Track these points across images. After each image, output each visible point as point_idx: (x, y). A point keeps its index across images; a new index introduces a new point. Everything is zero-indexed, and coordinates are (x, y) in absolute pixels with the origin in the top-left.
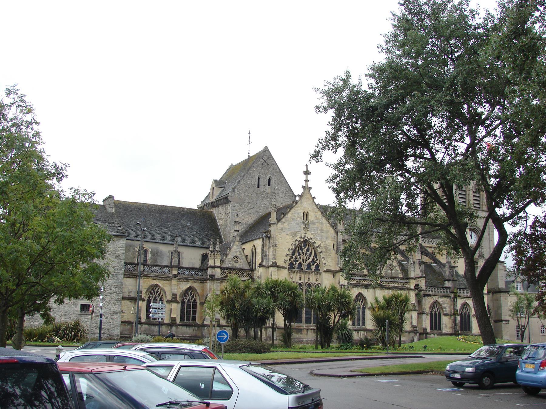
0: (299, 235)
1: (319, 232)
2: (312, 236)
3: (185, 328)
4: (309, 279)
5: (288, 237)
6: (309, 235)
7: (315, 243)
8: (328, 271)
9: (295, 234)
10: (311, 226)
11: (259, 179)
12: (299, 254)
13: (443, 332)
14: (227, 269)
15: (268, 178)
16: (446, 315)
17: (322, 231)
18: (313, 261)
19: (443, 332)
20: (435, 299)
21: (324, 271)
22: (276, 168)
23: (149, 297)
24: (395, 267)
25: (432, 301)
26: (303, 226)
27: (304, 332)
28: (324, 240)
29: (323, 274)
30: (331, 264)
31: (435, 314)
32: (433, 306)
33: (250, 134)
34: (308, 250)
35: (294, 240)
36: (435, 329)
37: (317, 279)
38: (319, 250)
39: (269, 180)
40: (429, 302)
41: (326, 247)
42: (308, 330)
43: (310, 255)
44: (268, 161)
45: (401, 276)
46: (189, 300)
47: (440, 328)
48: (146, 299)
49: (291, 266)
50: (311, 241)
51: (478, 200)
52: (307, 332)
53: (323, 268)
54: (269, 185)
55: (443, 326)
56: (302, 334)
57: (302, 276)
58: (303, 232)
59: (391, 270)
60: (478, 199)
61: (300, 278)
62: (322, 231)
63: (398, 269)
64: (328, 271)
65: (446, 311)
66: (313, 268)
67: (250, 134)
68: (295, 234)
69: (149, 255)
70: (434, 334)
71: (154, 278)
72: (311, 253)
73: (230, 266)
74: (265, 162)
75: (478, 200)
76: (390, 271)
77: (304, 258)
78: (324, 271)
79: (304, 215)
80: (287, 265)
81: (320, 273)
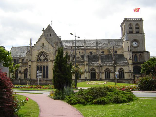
0: (40, 50)
1: (47, 49)
2: (45, 50)
3: (16, 81)
4: (44, 64)
5: (36, 52)
6: (44, 50)
7: (46, 52)
8: (51, 61)
9: (39, 50)
10: (44, 47)
11: (47, 35)
12: (41, 57)
13: (111, 79)
14: (24, 63)
15: (50, 34)
16: (112, 73)
17: (48, 48)
18: (46, 58)
19: (111, 79)
20: (107, 67)
21: (49, 61)
22: (52, 30)
23: (106, 72)
24: (80, 57)
25: (106, 68)
26: (41, 48)
27: (42, 81)
28: (49, 51)
29: (49, 62)
30: (52, 59)
31: (93, 73)
32: (106, 70)
33: (52, 21)
34: (44, 55)
35: (38, 52)
36: (107, 78)
37: (47, 64)
38: (47, 55)
39: (51, 35)
40: (104, 69)
41: (50, 54)
42: (43, 80)
43: (45, 56)
44: (50, 29)
45: (82, 60)
46: (107, 72)
47: (109, 77)
48: (105, 72)
49: (38, 60)
50: (44, 52)
51: (132, 31)
52: (43, 81)
53: (49, 60)
54: (51, 36)
55: (111, 77)
56: (41, 81)
57: (42, 63)
58: (42, 49)
59: (78, 59)
60: (132, 31)
61: (41, 64)
62: (48, 48)
63: (81, 58)
64: (51, 61)
65: (112, 71)
66: (46, 60)
67: (52, 21)
68: (39, 50)
69: (16, 61)
70: (107, 80)
71: (106, 66)
72: (45, 56)
73: (25, 62)
74: (49, 29)
75: (132, 31)
76: (77, 59)
77: (42, 57)
78: (49, 61)
79: (42, 44)
80: (36, 60)
81: (48, 62)
